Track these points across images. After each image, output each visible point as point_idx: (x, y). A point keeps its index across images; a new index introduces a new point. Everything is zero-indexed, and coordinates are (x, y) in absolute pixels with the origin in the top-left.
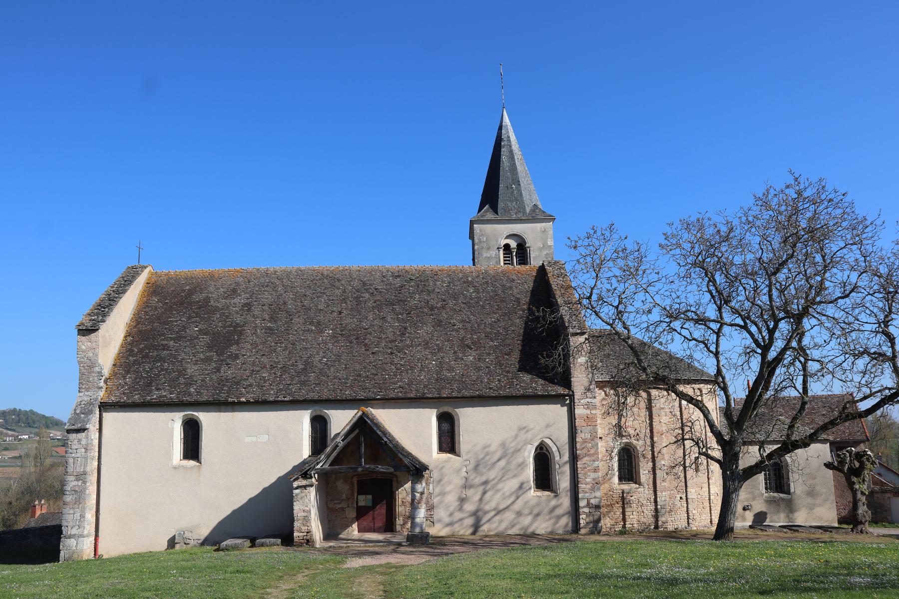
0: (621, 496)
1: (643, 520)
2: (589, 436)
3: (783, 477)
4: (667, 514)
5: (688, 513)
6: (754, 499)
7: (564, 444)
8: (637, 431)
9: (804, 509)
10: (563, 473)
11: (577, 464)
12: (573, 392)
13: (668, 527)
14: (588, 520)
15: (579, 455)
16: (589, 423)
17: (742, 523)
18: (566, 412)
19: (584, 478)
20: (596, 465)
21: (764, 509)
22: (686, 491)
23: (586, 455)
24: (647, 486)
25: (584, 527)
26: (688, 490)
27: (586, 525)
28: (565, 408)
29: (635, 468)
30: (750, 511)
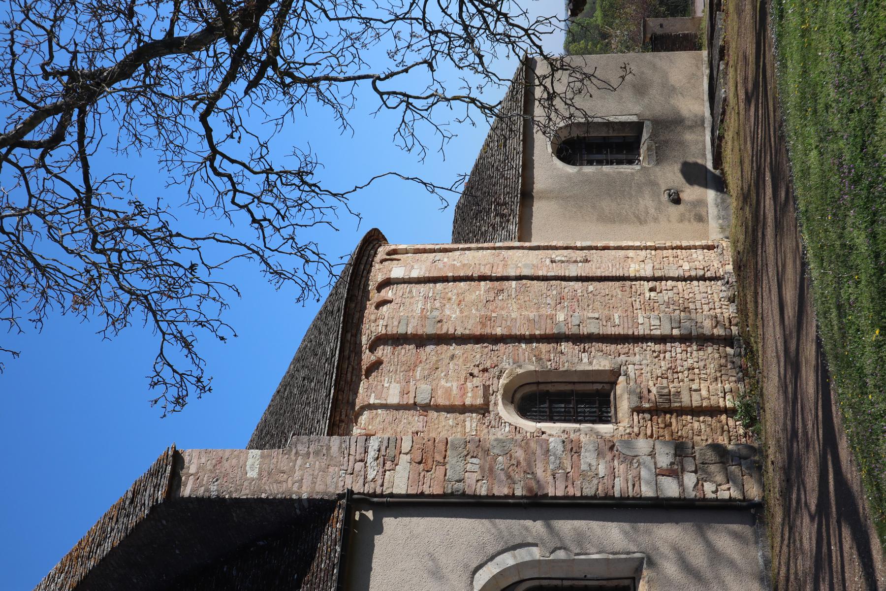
0: (647, 416)
1: (712, 368)
2: (474, 460)
3: (604, 137)
4: (693, 316)
5: (691, 279)
6: (653, 184)
7: (493, 530)
8: (476, 371)
9: (672, 101)
10: (580, 538)
11: (555, 497)
12: (340, 496)
13: (726, 315)
14: (720, 478)
15: (530, 490)
16: (438, 458)
17: (709, 206)
18: (399, 519)
19: (595, 481)
20: (560, 447)
21: (677, 167)
22: (636, 279)
23: (530, 471)
24: (623, 358)
25: (742, 488)
26: (632, 275)
27: (735, 483)
28: (389, 522)
29: (574, 383)
30: (682, 191)
